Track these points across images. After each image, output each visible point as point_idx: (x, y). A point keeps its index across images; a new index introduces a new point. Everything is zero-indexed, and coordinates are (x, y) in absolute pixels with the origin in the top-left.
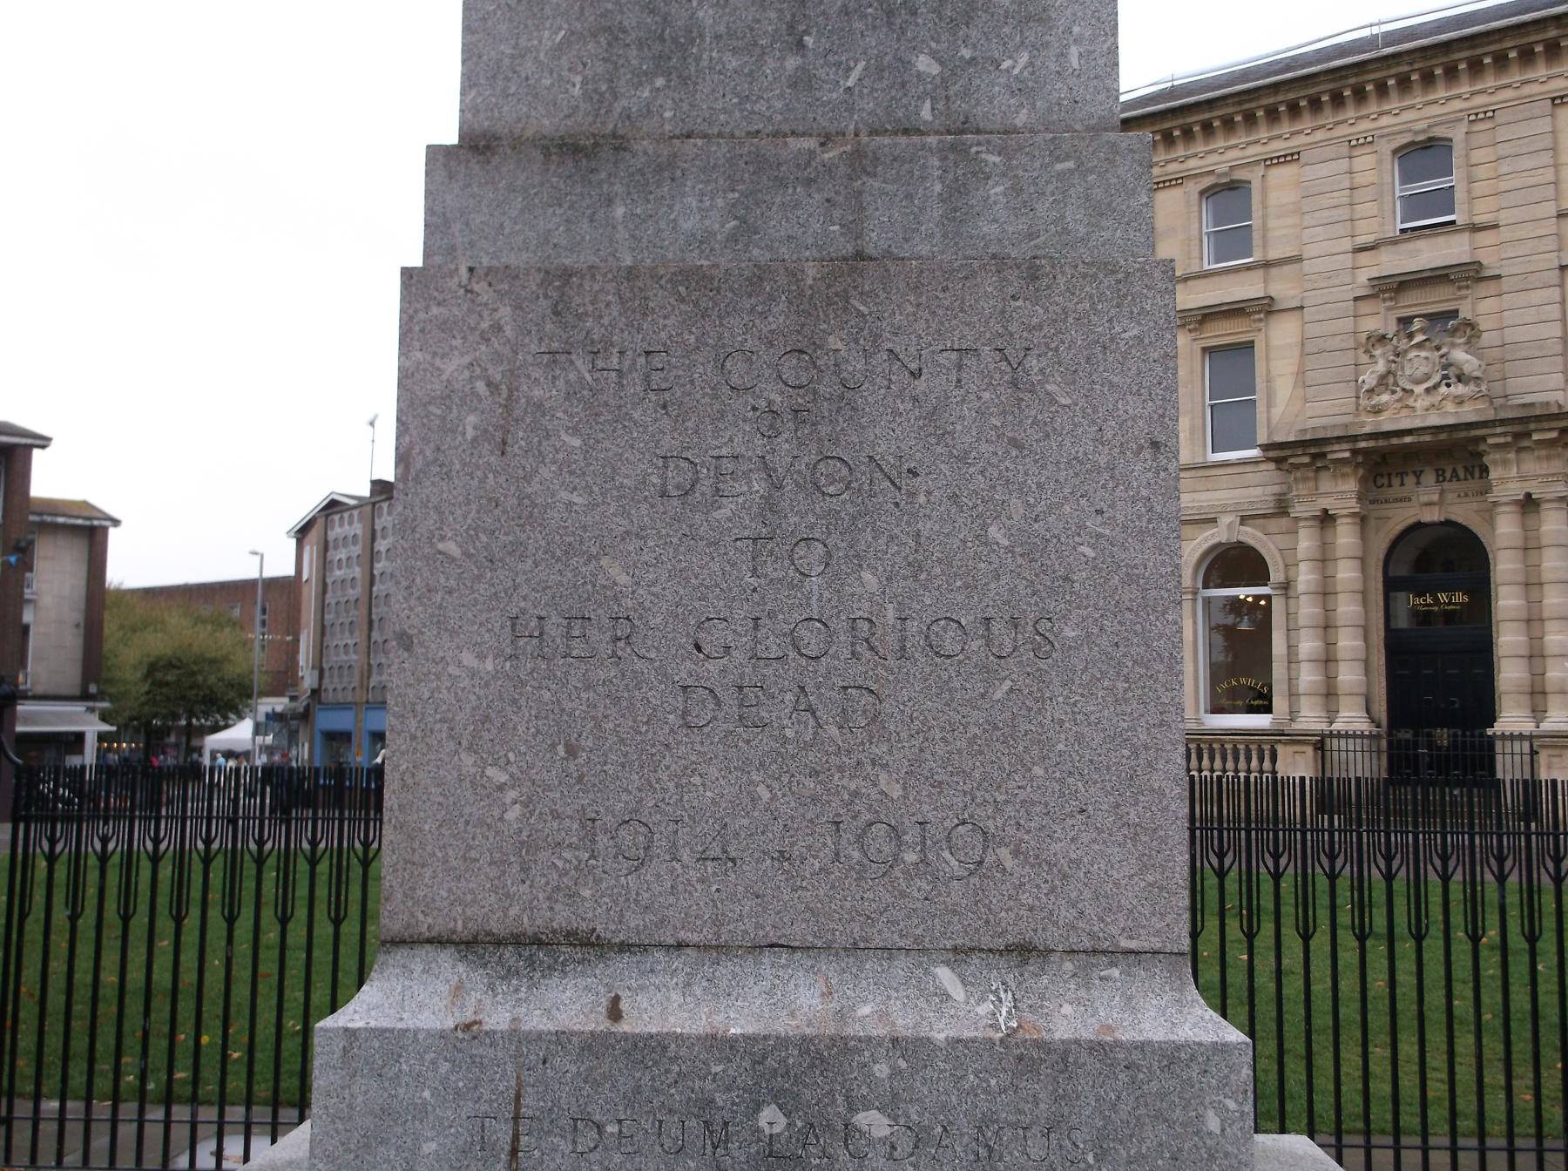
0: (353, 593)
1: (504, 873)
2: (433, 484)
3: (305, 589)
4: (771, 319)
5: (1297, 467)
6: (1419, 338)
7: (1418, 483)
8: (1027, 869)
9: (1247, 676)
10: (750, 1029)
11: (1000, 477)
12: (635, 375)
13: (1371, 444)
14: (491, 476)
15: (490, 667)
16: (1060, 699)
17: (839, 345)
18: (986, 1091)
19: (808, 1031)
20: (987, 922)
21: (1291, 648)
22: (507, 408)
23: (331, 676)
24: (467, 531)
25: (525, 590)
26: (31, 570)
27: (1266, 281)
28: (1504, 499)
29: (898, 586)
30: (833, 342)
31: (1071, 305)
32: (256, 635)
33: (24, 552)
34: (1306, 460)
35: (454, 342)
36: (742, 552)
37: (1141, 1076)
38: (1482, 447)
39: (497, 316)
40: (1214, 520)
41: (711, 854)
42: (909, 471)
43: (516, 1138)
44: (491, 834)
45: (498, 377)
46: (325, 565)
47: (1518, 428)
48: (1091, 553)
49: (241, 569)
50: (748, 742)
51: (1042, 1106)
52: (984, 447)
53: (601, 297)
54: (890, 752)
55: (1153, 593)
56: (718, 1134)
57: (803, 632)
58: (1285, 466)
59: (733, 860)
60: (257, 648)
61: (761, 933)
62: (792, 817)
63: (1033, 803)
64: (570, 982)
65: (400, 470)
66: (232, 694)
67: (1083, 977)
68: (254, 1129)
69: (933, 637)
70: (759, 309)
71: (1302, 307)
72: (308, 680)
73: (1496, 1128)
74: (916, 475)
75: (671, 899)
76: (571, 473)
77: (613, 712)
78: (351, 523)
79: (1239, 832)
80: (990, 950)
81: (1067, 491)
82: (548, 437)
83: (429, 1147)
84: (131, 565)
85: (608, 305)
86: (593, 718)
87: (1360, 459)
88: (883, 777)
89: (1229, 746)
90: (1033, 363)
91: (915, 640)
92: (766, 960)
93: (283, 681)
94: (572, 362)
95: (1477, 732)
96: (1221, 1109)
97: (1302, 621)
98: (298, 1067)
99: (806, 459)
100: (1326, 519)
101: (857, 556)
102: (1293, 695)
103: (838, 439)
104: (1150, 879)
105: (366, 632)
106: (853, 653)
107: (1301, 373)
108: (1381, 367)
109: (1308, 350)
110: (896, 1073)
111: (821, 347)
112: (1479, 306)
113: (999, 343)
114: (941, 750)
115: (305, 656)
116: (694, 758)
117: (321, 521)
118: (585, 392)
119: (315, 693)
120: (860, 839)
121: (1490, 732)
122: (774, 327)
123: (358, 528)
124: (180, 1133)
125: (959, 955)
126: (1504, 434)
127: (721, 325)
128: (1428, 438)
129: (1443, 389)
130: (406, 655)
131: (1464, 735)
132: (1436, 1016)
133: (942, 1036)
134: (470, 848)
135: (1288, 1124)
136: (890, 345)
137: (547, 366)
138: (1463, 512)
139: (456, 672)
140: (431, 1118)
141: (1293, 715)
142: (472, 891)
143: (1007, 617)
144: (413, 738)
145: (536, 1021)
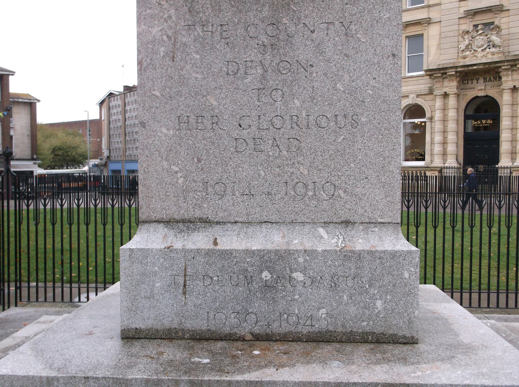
0: (119, 124)
1: (178, 200)
2: (150, 71)
3: (103, 123)
4: (263, 13)
5: (437, 77)
6: (480, 32)
7: (477, 83)
8: (348, 197)
9: (417, 148)
10: (259, 248)
11: (341, 67)
12: (217, 33)
13: (462, 69)
14: (169, 68)
15: (171, 133)
16: (360, 142)
17: (287, 22)
18: (335, 266)
19: (277, 248)
20: (335, 214)
21: (432, 139)
22: (174, 45)
23: (113, 152)
24: (162, 87)
25: (182, 107)
26: (12, 117)
27: (428, 12)
28: (506, 88)
29: (307, 104)
30: (285, 21)
31: (366, 7)
32: (88, 139)
33: (9, 110)
34: (440, 75)
35: (155, 22)
36: (254, 94)
37: (384, 261)
38: (500, 70)
39: (170, 13)
40: (408, 96)
41: (245, 193)
42: (310, 65)
43: (185, 281)
44: (174, 187)
45: (171, 34)
46: (109, 115)
47: (512, 63)
48: (371, 93)
49: (82, 117)
50: (257, 156)
51: (352, 270)
52: (336, 57)
53: (205, 5)
54: (304, 159)
55: (392, 106)
56: (249, 280)
57: (275, 120)
58: (433, 77)
59: (253, 195)
60: (88, 143)
61: (262, 218)
62: (272, 181)
63: (351, 176)
64: (200, 234)
65: (139, 67)
66: (81, 158)
67: (366, 231)
68: (99, 290)
69: (318, 121)
70: (259, 9)
71: (440, 21)
72: (106, 153)
73: (493, 288)
74: (313, 66)
75: (233, 208)
76: (197, 67)
77: (212, 147)
78: (117, 100)
79: (415, 190)
80: (336, 223)
81: (364, 71)
82: (188, 55)
83: (158, 285)
84: (44, 117)
85: (207, 8)
86: (206, 149)
87: (458, 74)
88: (301, 167)
89: (410, 172)
90: (353, 27)
91: (312, 122)
92: (264, 227)
93: (97, 154)
94: (196, 29)
95: (493, 166)
96: (409, 271)
97: (436, 130)
98: (111, 272)
99: (275, 62)
100: (446, 95)
101: (293, 94)
102: (432, 155)
103: (286, 54)
104: (388, 199)
105: (124, 137)
106: (291, 127)
107: (439, 44)
108: (467, 42)
109: (442, 36)
110: (306, 261)
111: (280, 23)
112: (501, 20)
113: (341, 20)
114: (320, 158)
115: (104, 146)
116: (239, 162)
117: (107, 100)
118: (200, 39)
119: (108, 157)
120: (294, 188)
121: (497, 166)
122: (264, 15)
123: (120, 102)
124: (75, 291)
125: (326, 224)
126: (507, 65)
127: (246, 15)
128: (481, 67)
129: (488, 50)
130: (143, 129)
131: (488, 167)
132: (476, 255)
133: (320, 249)
134: (167, 192)
135: (427, 282)
136: (304, 22)
137: (187, 30)
138: (492, 92)
139: (160, 135)
140: (158, 276)
141: (432, 161)
142: (168, 206)
143: (343, 115)
144: (147, 156)
145: (190, 246)
